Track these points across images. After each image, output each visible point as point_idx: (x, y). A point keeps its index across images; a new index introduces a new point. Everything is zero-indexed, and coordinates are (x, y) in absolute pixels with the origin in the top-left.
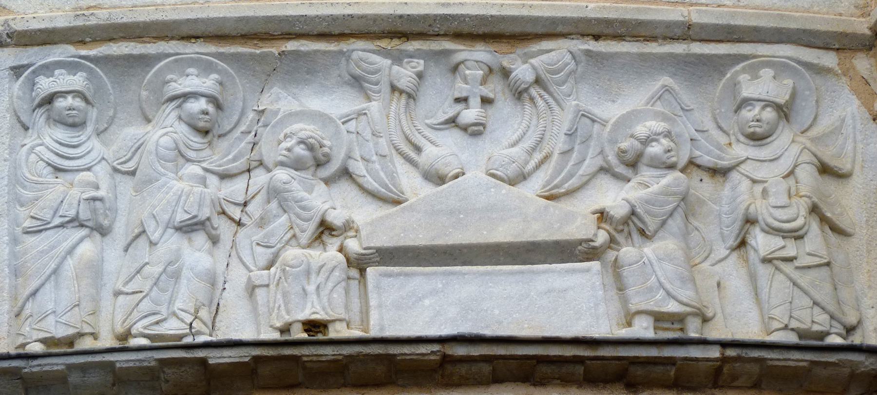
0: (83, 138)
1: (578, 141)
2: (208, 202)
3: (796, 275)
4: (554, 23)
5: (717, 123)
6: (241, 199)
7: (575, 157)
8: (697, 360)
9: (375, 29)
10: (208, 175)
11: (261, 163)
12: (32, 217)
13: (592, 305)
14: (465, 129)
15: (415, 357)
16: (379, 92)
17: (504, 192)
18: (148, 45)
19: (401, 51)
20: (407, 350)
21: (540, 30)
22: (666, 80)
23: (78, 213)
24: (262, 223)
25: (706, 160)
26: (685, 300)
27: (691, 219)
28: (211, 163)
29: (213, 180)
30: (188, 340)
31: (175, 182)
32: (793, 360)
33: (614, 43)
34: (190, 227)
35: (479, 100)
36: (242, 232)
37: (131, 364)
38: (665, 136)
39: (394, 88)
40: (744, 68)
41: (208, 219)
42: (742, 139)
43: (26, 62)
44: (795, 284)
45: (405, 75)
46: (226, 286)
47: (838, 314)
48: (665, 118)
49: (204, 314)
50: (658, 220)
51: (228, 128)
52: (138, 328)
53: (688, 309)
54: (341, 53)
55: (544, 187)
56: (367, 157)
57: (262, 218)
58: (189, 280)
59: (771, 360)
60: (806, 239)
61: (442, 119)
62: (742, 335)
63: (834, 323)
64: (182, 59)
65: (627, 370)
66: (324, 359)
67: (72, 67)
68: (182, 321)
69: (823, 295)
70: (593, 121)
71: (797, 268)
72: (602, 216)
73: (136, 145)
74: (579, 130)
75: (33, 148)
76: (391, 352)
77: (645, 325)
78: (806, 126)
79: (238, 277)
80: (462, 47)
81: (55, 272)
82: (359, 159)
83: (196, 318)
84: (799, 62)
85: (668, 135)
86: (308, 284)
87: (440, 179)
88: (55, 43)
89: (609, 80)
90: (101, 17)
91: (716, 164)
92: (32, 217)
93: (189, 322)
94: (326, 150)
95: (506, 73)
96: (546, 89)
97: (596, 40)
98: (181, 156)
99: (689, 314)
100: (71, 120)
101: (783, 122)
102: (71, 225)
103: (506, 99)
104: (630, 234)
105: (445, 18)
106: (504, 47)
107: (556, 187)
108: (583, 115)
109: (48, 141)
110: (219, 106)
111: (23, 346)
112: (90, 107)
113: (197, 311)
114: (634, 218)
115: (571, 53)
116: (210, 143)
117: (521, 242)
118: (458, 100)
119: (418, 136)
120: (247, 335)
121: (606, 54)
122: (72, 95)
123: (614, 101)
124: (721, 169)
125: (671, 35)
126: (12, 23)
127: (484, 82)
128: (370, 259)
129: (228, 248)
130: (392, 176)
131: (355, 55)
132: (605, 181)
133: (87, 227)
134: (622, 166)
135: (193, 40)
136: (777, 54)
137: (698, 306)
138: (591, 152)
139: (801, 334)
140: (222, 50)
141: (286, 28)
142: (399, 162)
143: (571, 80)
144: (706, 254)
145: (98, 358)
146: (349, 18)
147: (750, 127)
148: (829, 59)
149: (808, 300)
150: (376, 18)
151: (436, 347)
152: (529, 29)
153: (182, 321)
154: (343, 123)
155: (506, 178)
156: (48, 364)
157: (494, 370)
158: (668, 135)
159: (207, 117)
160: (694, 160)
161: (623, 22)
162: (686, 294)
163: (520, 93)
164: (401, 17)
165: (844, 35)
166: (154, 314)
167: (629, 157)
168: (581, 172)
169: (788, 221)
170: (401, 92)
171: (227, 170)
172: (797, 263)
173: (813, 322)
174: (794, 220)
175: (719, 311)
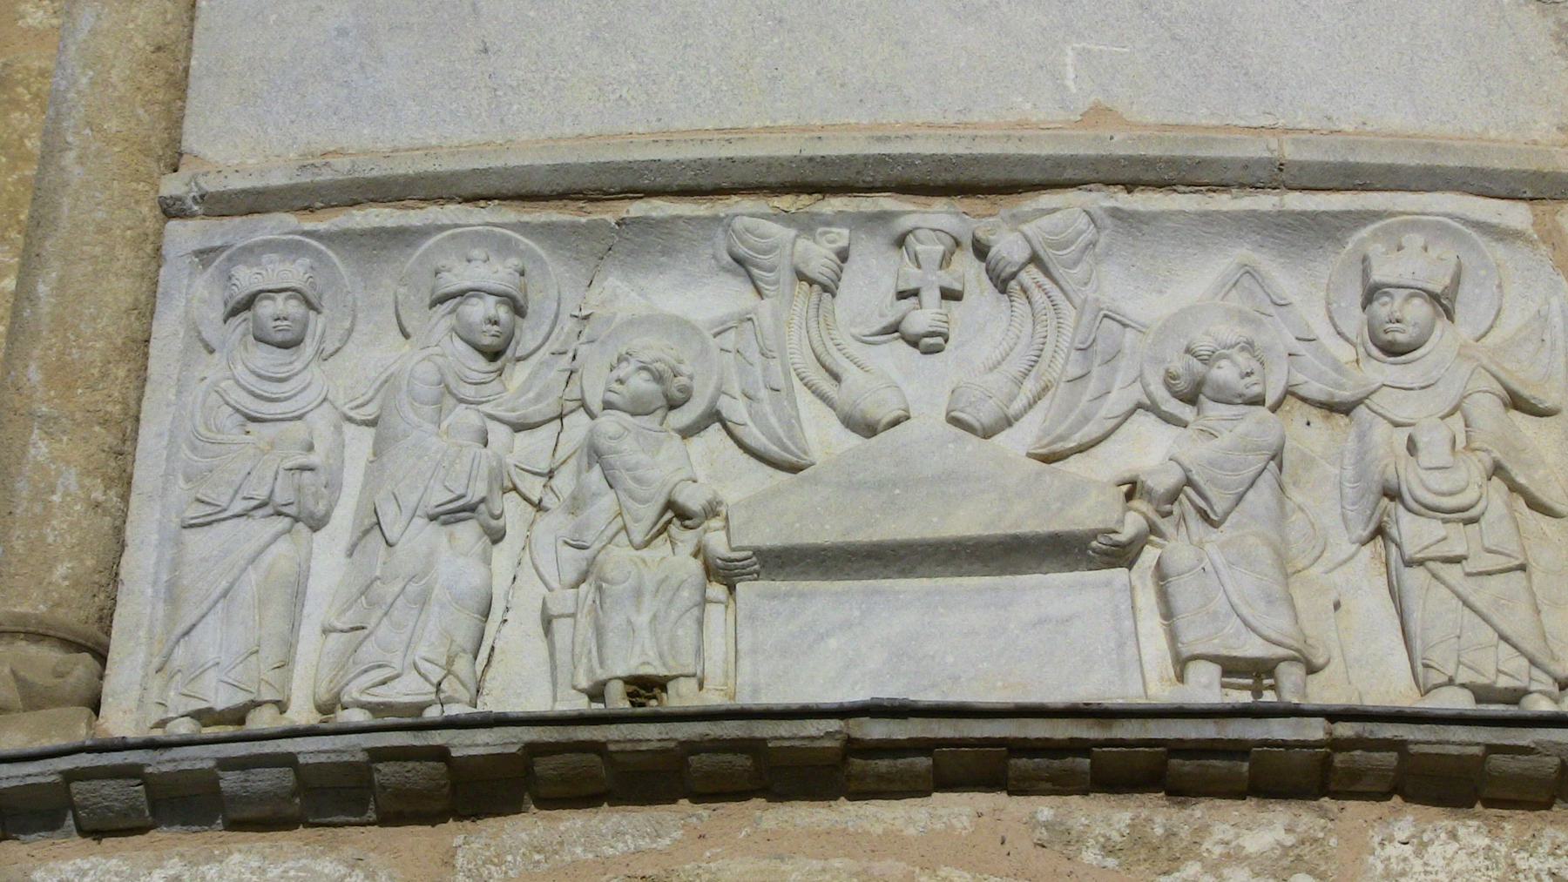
0: (298, 366)
1: (1098, 360)
2: (484, 471)
3: (1467, 587)
4: (1059, 165)
5: (1335, 326)
6: (544, 467)
7: (1093, 386)
8: (1284, 744)
9: (771, 180)
10: (492, 426)
11: (583, 405)
12: (199, 500)
13: (1112, 645)
14: (914, 342)
15: (797, 743)
16: (776, 282)
17: (969, 448)
18: (412, 212)
19: (812, 216)
20: (784, 729)
21: (1037, 176)
22: (1242, 252)
23: (272, 492)
24: (576, 504)
25: (1314, 389)
26: (1274, 636)
27: (1292, 491)
28: (498, 405)
29: (499, 433)
30: (432, 713)
31: (434, 439)
32: (1454, 743)
33: (1158, 195)
34: (455, 513)
35: (938, 293)
36: (544, 522)
37: (323, 758)
38: (1243, 349)
39: (801, 276)
40: (1375, 235)
41: (483, 500)
42: (1375, 352)
43: (218, 243)
44: (1466, 603)
45: (817, 254)
46: (509, 616)
47: (1542, 658)
48: (1244, 319)
49: (462, 666)
50: (1230, 498)
51: (533, 346)
52: (353, 693)
53: (1281, 652)
54: (716, 219)
55: (1040, 439)
56: (751, 393)
57: (574, 498)
58: (442, 606)
59: (1417, 743)
60: (1483, 522)
61: (877, 327)
62: (1374, 699)
63: (1536, 673)
64: (462, 234)
65: (1165, 763)
66: (644, 747)
67: (290, 249)
68: (426, 679)
69: (1517, 622)
70: (1125, 325)
71: (1469, 575)
72: (1133, 489)
73: (383, 377)
74: (1099, 341)
75: (216, 384)
76: (757, 734)
77: (1204, 680)
78: (1482, 330)
79: (530, 597)
80: (909, 207)
81: (224, 595)
82: (738, 394)
83: (449, 672)
84: (1466, 222)
85: (1249, 347)
86: (638, 611)
87: (868, 429)
88: (268, 211)
89: (1152, 257)
90: (341, 169)
91: (1332, 395)
92: (199, 500)
93: (435, 681)
94: (683, 380)
95: (981, 250)
96: (1047, 273)
97: (1129, 192)
98: (447, 393)
99: (1284, 659)
100: (279, 337)
101: (1442, 324)
102: (261, 512)
103: (982, 292)
104: (1183, 517)
105: (882, 160)
106: (978, 204)
107: (1061, 438)
108: (1106, 316)
109: (240, 370)
110: (518, 310)
111: (162, 724)
112: (312, 314)
113: (451, 660)
114: (1188, 490)
115: (1088, 213)
116: (500, 372)
117: (995, 536)
118: (902, 295)
119: (837, 355)
120: (539, 703)
121: (1144, 214)
122: (284, 295)
123: (1161, 292)
124: (1341, 404)
125: (1252, 180)
126: (202, 181)
127: (945, 261)
128: (743, 567)
129: (518, 548)
130: (792, 423)
131: (738, 224)
132: (1144, 423)
133: (287, 515)
134: (1175, 402)
135: (482, 203)
136: (1429, 210)
137: (1296, 645)
138: (1120, 379)
139: (1482, 694)
140: (526, 218)
141: (629, 181)
142: (804, 398)
143: (1088, 258)
144: (1316, 552)
145: (269, 747)
146: (729, 163)
147: (1386, 332)
148: (1516, 215)
149: (1490, 631)
150: (770, 163)
151: (834, 725)
152: (1020, 175)
153: (426, 679)
154: (715, 336)
155: (976, 424)
156: (187, 759)
157: (935, 764)
158: (1249, 347)
159: (496, 328)
160: (1295, 389)
161: (1171, 162)
162: (1278, 623)
163: (1006, 282)
164: (811, 159)
165: (1539, 176)
166: (380, 666)
167: (1182, 385)
168: (1103, 413)
169: (1451, 494)
170: (811, 282)
171: (525, 416)
172: (1469, 566)
173: (1499, 671)
174: (1462, 490)
175: (1336, 653)
